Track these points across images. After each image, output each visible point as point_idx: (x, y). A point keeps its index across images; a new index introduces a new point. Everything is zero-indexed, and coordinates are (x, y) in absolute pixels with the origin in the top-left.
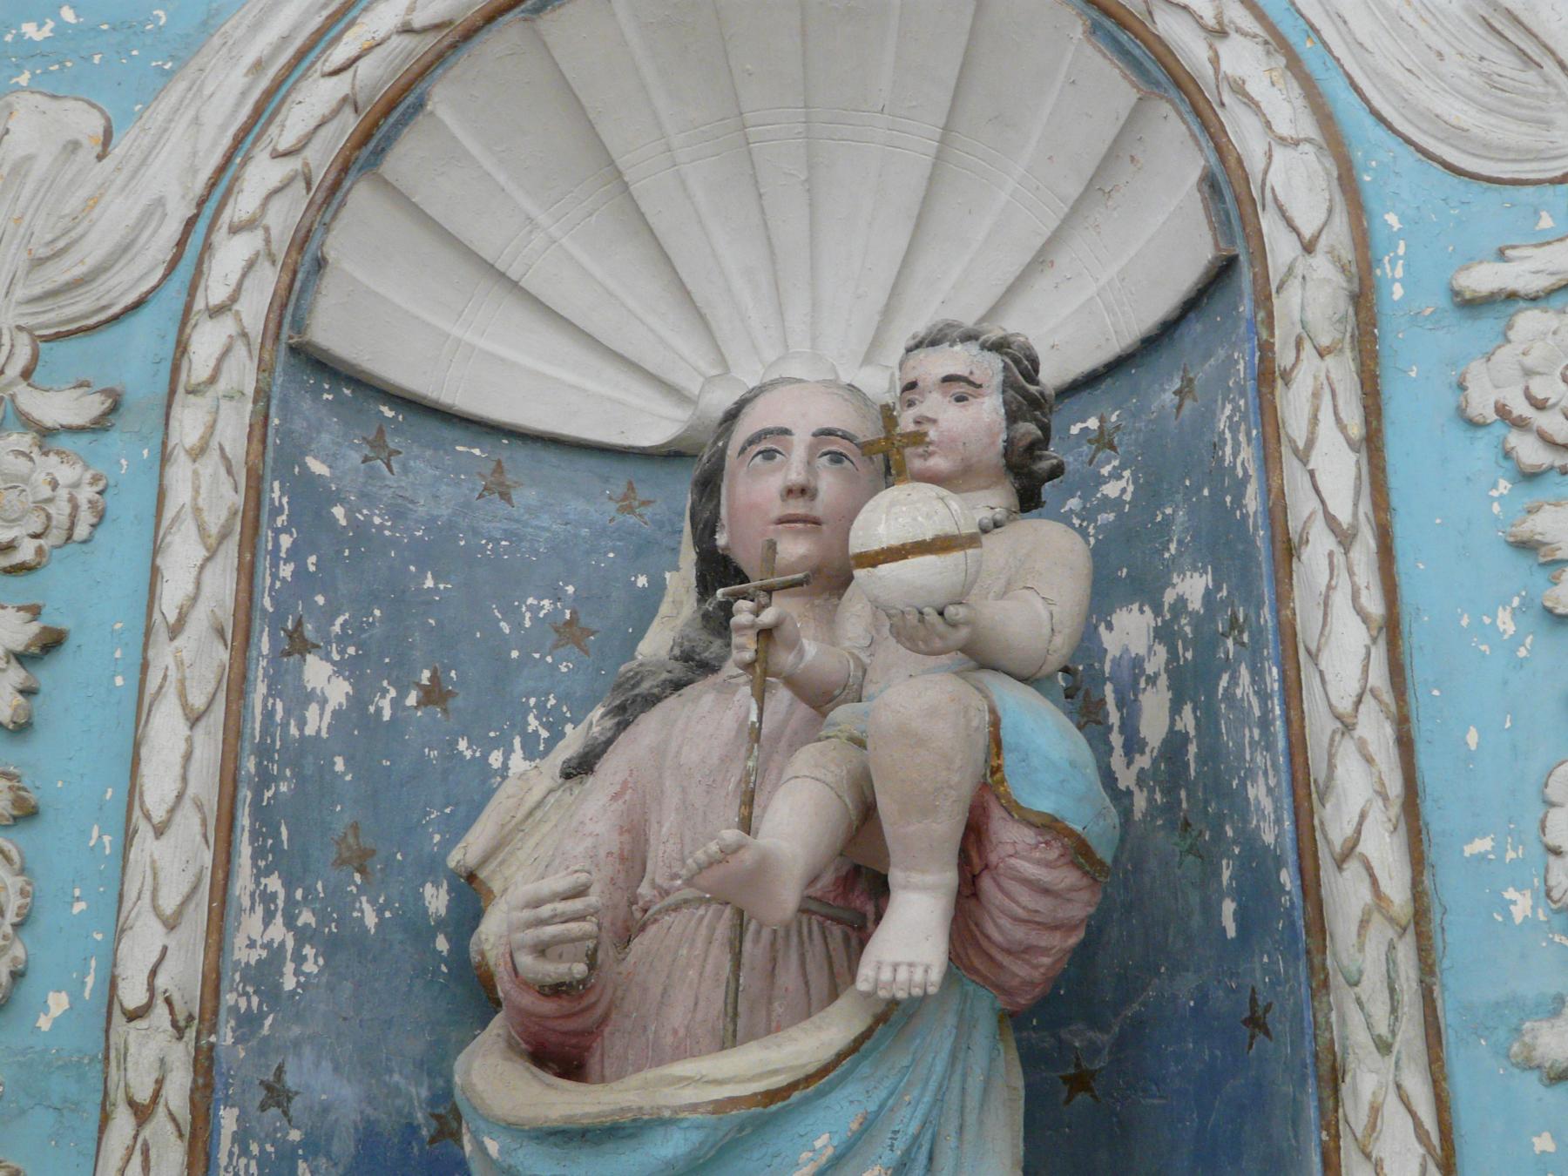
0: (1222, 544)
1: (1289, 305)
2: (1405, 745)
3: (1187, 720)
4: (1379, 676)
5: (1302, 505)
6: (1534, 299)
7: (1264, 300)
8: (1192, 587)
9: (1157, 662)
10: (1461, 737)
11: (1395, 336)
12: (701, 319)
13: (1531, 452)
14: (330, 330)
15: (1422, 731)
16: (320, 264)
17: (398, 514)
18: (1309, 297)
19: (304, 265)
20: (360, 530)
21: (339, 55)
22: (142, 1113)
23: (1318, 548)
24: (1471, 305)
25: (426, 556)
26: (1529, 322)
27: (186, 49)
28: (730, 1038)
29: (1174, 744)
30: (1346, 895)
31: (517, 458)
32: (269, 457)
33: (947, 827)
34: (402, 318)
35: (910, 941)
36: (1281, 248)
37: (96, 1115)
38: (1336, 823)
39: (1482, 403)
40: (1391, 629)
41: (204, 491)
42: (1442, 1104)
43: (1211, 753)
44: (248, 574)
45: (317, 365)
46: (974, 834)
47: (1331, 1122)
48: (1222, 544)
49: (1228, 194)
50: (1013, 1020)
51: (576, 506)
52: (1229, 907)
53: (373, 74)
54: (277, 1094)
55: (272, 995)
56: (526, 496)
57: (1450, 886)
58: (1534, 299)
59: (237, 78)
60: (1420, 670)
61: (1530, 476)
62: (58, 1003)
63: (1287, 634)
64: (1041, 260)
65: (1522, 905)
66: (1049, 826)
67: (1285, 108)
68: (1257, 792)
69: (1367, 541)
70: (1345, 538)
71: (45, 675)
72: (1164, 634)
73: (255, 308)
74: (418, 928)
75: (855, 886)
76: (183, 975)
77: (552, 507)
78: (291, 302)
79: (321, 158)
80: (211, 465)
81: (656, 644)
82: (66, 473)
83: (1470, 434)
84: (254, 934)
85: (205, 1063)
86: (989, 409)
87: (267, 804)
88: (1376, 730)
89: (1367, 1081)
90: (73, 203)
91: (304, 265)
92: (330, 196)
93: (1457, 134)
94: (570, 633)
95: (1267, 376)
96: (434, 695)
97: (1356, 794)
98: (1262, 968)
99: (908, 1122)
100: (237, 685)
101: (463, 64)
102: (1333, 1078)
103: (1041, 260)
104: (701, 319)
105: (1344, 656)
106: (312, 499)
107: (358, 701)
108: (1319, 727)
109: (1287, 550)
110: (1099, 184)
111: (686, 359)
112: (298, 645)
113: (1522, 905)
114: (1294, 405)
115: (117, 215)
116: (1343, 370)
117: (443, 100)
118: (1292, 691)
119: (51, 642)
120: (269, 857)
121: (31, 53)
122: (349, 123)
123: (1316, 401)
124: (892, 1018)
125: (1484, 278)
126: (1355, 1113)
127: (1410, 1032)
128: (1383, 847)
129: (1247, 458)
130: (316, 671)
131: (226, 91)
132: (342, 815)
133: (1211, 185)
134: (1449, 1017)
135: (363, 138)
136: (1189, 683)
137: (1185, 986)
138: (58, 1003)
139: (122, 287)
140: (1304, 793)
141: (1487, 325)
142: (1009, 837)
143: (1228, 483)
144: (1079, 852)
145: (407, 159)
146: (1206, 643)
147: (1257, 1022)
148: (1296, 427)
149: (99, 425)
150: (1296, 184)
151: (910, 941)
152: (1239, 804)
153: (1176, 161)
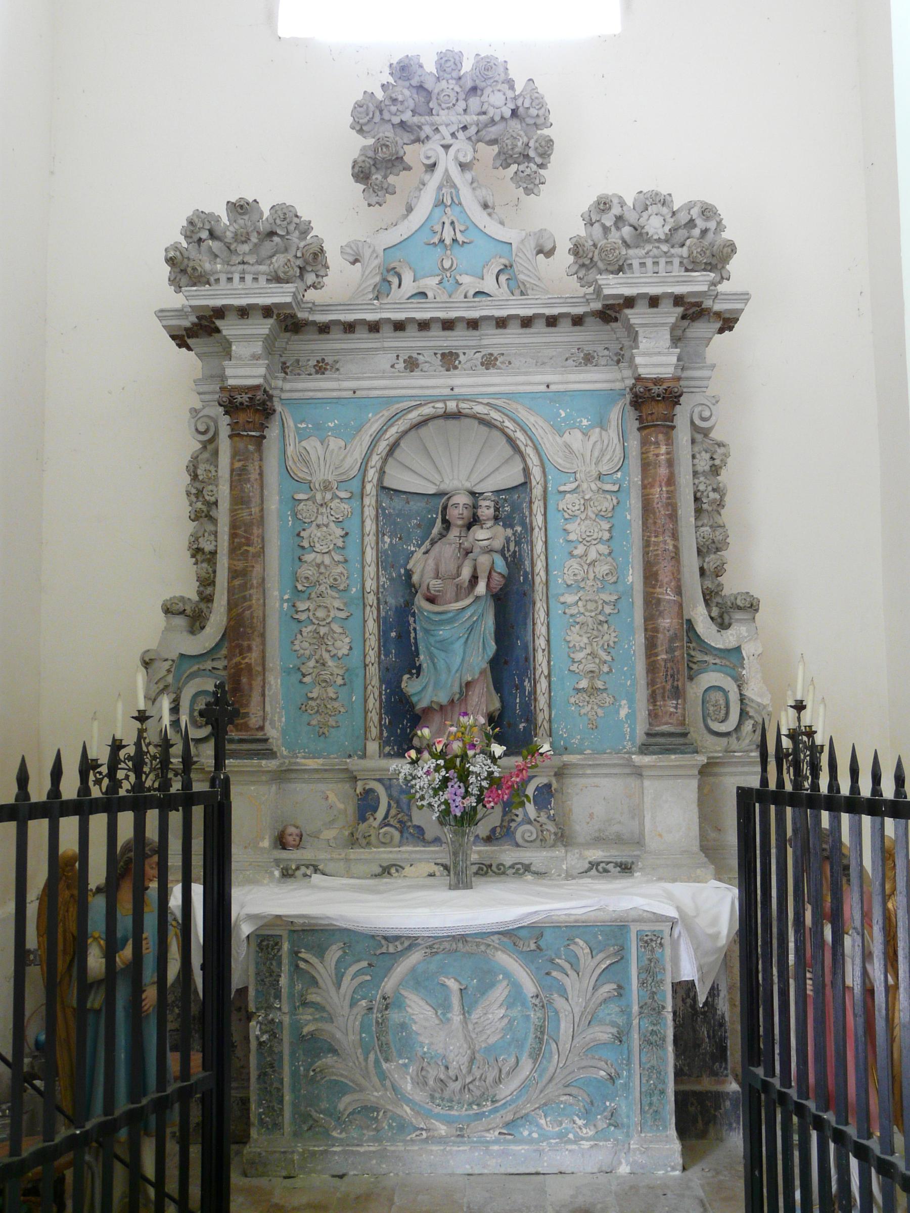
0: (523, 524)
1: (534, 491)
2: (547, 558)
3: (517, 549)
4: (544, 550)
5: (534, 524)
6: (569, 492)
7: (531, 490)
8: (519, 529)
9: (513, 538)
10: (554, 558)
11: (549, 496)
12: (439, 472)
13: (567, 516)
14: (385, 484)
15: (549, 556)
16: (384, 472)
17: (394, 509)
18: (537, 491)
19: (382, 472)
20: (389, 513)
21: (387, 437)
22: (371, 606)
23: (536, 530)
24: (560, 492)
25: (398, 516)
26: (568, 496)
27: (359, 429)
28: (457, 601)
29: (515, 552)
30: (537, 580)
31: (410, 496)
32: (378, 506)
33: (487, 574)
34: (399, 479)
35: (481, 588)
36: (534, 483)
37: (362, 606)
38: (537, 570)
39: (560, 508)
40: (546, 543)
41: (370, 512)
42: (548, 607)
43: (520, 555)
44: (377, 525)
45: (384, 488)
46: (490, 573)
47: (534, 610)
48: (523, 524)
49: (526, 471)
50: (492, 596)
51: (419, 504)
52: (518, 701)
53: (392, 440)
54: (386, 603)
55: (384, 588)
56: (412, 503)
57: (551, 578)
58: (569, 492)
59: (368, 437)
60: (550, 550)
61: (566, 519)
62: (354, 590)
63: (532, 542)
64: (497, 469)
65: (560, 581)
66: (499, 573)
67: (536, 461)
68: (526, 562)
69: (543, 529)
70: (541, 529)
71: (345, 539)
72: (514, 534)
73: (375, 481)
74: (400, 576)
75: (474, 580)
76: (374, 587)
77: (416, 505)
78: (380, 480)
79: (384, 454)
80: (371, 508)
81: (435, 531)
82: (346, 506)
83: (608, 327)
84: (382, 579)
85: (378, 599)
86: (492, 510)
87: (385, 561)
88: (543, 557)
89: (538, 605)
90: (341, 458)
91: (382, 472)
92: (385, 461)
93: (560, 464)
94: (419, 526)
95: (531, 502)
96: (400, 539)
97: (540, 566)
98: (526, 587)
99: (480, 611)
100: (377, 543)
101: (406, 437)
102: (534, 604)
103: (497, 469)
104: (439, 472)
105: (539, 547)
106: (384, 509)
107: (391, 541)
108: (535, 556)
109: (532, 529)
110: (507, 461)
111: (437, 478)
112: (384, 535)
113: (560, 581)
114: (535, 507)
115: (349, 462)
116: (541, 503)
117: (402, 444)
118: (532, 550)
119: (347, 534)
120: (384, 569)
121: (330, 429)
122: (388, 448)
123: (538, 506)
124: (478, 598)
125: (562, 488)
126: (537, 608)
127: (544, 598)
128: (543, 574)
129: (527, 513)
130: (386, 537)
131: (366, 440)
132: (390, 560)
133: (524, 470)
134: (550, 596)
135: (390, 450)
136: (518, 543)
137: (515, 587)
138: (354, 590)
139: (353, 473)
140: (533, 565)
141: (562, 495)
142: (494, 574)
143: (524, 516)
144: (503, 576)
145: (397, 453)
146: (521, 539)
147: (525, 594)
148: (535, 512)
149: (350, 498)
150: (536, 472)
151: (481, 588)
152: (524, 565)
153: (519, 466)
